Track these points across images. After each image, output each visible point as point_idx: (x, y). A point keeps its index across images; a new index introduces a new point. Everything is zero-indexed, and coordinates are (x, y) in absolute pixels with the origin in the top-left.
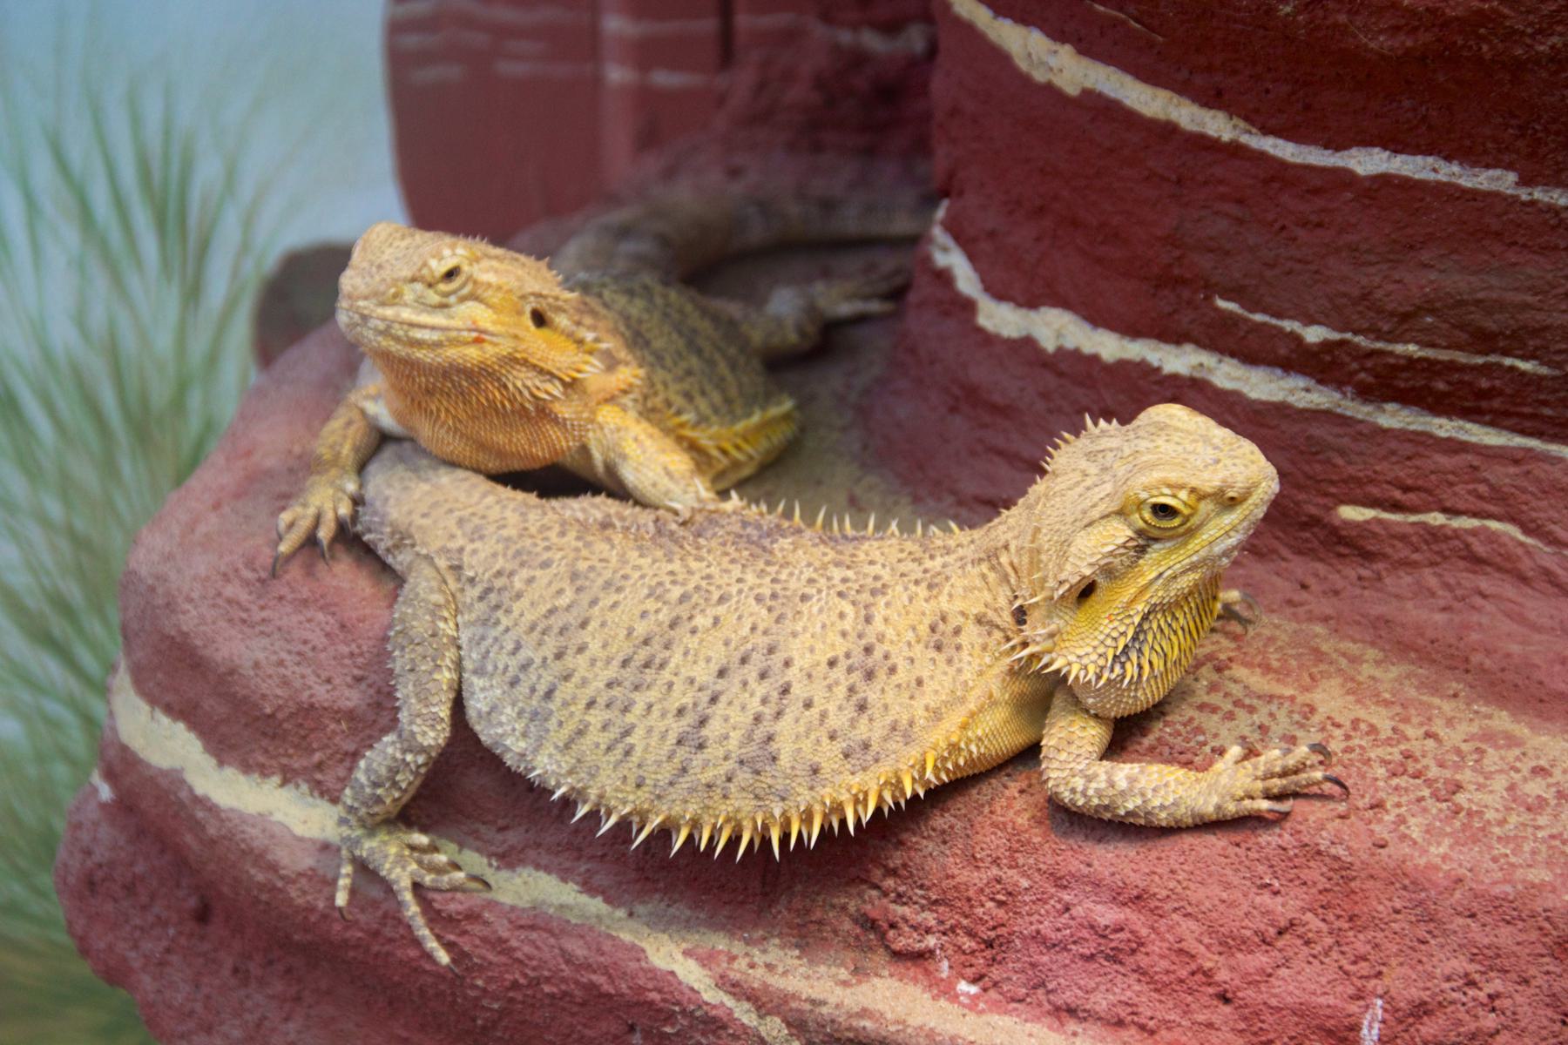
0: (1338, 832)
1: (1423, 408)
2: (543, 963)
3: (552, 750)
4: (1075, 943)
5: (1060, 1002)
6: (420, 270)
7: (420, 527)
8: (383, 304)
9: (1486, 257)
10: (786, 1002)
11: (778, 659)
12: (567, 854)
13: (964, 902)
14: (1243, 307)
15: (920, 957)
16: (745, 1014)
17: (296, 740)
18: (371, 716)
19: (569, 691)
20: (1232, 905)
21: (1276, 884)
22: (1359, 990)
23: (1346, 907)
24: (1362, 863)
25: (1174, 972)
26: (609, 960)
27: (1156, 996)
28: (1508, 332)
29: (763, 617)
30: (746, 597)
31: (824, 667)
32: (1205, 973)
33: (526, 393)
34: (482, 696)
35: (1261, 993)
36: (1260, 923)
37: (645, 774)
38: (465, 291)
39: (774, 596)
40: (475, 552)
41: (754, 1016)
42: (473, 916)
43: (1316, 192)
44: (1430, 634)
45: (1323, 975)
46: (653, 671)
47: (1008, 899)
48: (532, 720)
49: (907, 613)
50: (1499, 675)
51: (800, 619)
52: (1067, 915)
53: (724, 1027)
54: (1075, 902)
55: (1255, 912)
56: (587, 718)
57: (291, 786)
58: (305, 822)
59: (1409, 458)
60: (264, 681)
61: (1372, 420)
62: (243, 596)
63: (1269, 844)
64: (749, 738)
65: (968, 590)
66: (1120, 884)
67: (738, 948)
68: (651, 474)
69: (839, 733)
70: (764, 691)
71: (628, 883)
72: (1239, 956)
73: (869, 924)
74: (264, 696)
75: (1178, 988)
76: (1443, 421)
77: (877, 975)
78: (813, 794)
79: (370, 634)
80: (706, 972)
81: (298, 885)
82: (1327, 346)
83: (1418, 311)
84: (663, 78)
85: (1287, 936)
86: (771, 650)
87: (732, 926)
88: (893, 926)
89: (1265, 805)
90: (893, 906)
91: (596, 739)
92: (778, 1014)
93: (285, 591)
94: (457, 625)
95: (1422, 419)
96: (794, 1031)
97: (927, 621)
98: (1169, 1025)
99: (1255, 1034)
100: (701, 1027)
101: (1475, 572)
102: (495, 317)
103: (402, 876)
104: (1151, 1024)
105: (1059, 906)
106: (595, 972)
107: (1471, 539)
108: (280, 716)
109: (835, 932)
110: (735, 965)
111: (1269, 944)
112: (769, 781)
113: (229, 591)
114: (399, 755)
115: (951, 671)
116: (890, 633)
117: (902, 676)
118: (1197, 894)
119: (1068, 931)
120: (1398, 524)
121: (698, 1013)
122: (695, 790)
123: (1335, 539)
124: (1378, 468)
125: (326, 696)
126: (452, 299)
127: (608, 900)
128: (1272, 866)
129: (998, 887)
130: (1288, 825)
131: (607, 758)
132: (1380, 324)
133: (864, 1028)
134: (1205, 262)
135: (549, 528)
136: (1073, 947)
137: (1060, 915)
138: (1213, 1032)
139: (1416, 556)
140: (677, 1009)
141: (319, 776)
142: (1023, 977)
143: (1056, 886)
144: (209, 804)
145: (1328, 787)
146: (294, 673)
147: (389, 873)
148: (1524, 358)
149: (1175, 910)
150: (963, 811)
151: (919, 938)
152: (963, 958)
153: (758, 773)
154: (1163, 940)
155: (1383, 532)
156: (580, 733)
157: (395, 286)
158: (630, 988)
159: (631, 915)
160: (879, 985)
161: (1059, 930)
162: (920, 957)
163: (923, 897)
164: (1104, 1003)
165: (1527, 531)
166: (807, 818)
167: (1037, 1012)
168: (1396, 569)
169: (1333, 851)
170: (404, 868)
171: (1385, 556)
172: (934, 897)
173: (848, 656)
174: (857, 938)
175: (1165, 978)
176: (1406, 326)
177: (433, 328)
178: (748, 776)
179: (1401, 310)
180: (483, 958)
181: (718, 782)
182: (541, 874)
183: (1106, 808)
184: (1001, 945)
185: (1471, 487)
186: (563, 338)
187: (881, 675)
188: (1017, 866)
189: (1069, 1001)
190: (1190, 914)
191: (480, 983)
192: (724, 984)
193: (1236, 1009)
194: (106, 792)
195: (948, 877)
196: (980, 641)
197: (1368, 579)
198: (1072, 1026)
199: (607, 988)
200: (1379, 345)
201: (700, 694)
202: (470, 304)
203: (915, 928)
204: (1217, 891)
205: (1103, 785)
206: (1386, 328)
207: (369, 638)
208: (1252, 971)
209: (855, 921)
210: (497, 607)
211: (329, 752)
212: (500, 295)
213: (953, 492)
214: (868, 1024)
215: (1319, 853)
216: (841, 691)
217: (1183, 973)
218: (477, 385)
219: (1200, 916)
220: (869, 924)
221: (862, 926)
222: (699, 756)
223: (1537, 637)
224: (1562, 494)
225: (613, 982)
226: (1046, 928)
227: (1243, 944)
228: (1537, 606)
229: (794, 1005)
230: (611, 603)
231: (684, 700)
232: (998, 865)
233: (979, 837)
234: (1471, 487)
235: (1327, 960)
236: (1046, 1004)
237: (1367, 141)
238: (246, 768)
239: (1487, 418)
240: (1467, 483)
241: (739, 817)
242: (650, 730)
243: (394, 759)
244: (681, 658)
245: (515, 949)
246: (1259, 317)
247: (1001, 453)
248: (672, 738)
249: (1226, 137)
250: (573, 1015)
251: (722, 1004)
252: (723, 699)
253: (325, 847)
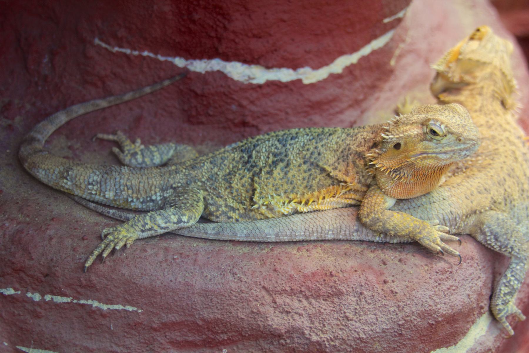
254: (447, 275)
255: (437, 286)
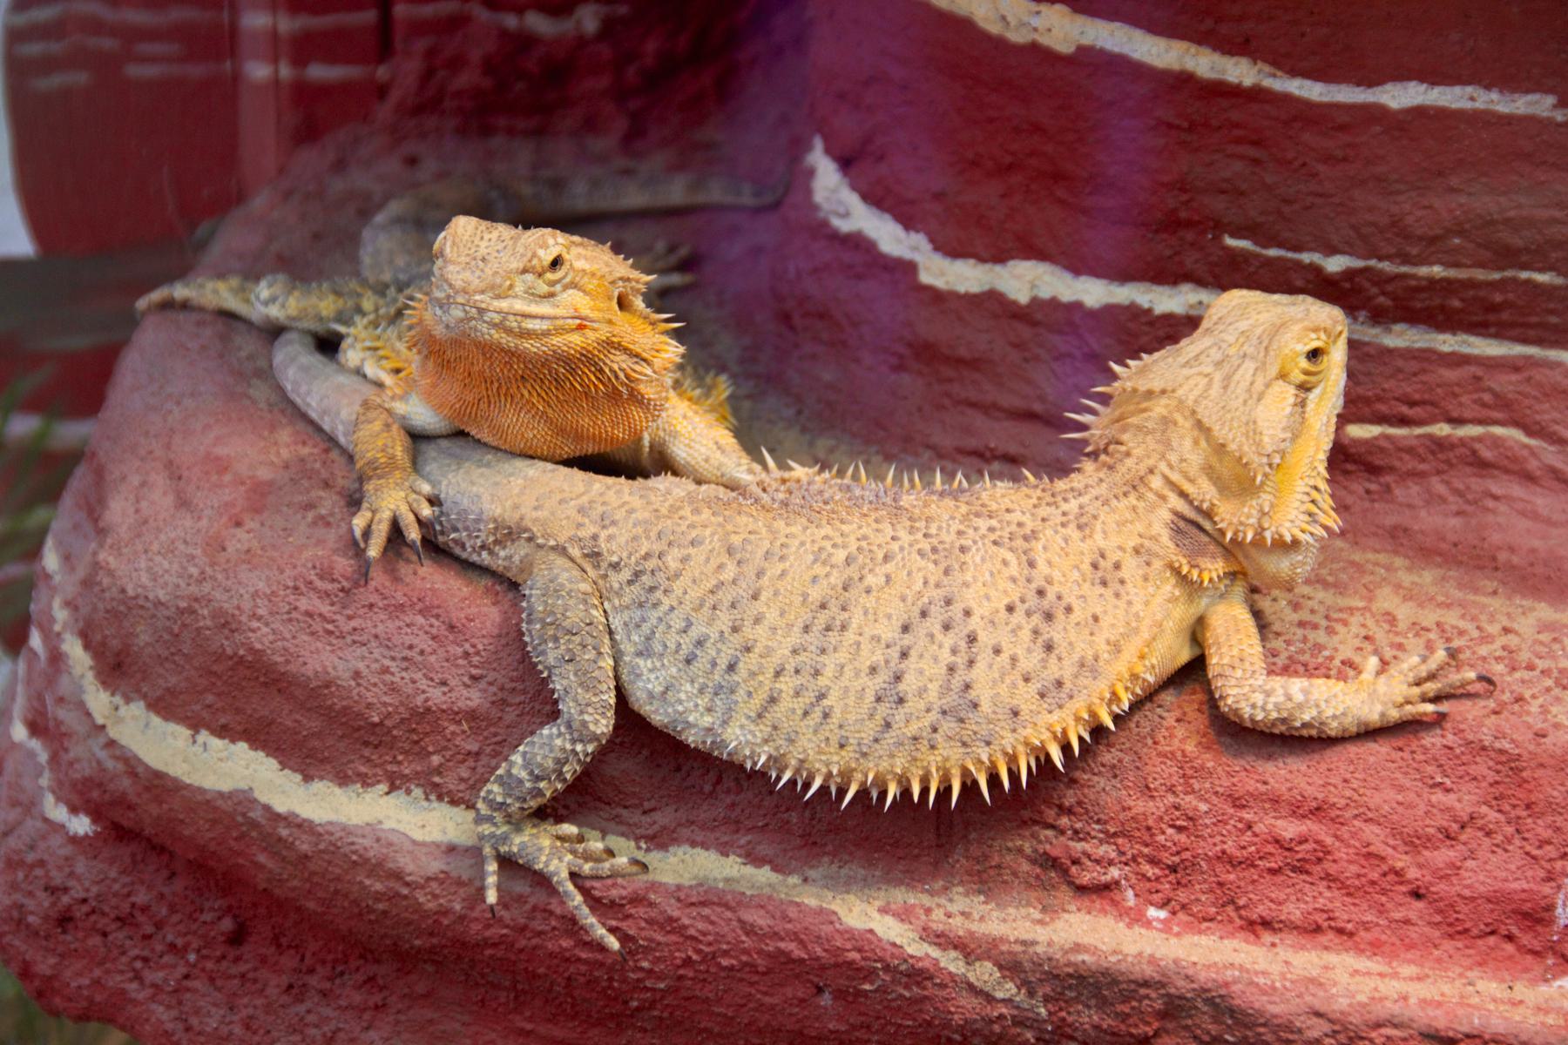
0: (1498, 729)
1: (1430, 326)
2: (720, 937)
3: (744, 721)
4: (1260, 858)
5: (1255, 917)
6: (530, 261)
7: (536, 520)
8: (498, 297)
9: (1515, 178)
10: (996, 946)
11: (957, 609)
12: (723, 828)
13: (1143, 831)
14: (1256, 243)
15: (1105, 889)
16: (951, 962)
17: (407, 746)
18: (495, 713)
19: (754, 661)
20: (1411, 806)
21: (1448, 782)
22: (1549, 872)
23: (1521, 796)
24: (1530, 753)
25: (1365, 875)
26: (798, 926)
27: (1348, 900)
28: (1533, 247)
29: (934, 573)
30: (909, 554)
31: (1003, 613)
32: (1397, 873)
33: (622, 375)
34: (652, 676)
35: (1453, 885)
36: (1442, 820)
37: (848, 734)
38: (567, 280)
39: (934, 550)
40: (610, 538)
41: (961, 963)
42: (637, 900)
43: (1342, 128)
44: (1451, 537)
45: (1511, 863)
46: (836, 633)
47: (1188, 823)
48: (716, 694)
49: (1067, 555)
50: (1529, 569)
51: (968, 569)
52: (1249, 833)
53: (931, 978)
54: (1256, 819)
55: (1435, 811)
56: (777, 685)
57: (401, 792)
58: (424, 826)
59: (1415, 374)
60: (369, 690)
61: (1378, 341)
62: (325, 609)
63: (1433, 744)
64: (946, 689)
65: (1121, 524)
66: (1299, 798)
67: (926, 900)
68: (703, 450)
69: (1033, 675)
70: (952, 642)
71: (792, 849)
72: (1426, 853)
73: (1049, 862)
74: (369, 706)
75: (1371, 890)
76: (1447, 337)
77: (1064, 911)
78: (1016, 736)
79: (484, 632)
80: (906, 926)
81: (428, 890)
82: (1349, 274)
83: (1449, 232)
84: (319, 72)
85: (1469, 830)
86: (948, 602)
87: (911, 879)
88: (1075, 862)
89: (1430, 708)
90: (1072, 844)
91: (790, 705)
92: (989, 958)
93: (374, 598)
94: (605, 611)
95: (1427, 337)
96: (1007, 973)
97: (1087, 560)
98: (1366, 926)
99: (1450, 925)
100: (904, 980)
101: (1482, 476)
102: (592, 303)
103: (558, 866)
104: (1350, 926)
105: (1240, 825)
106: (782, 939)
107: (1477, 446)
108: (388, 723)
109: (1015, 874)
110: (934, 917)
111: (1453, 839)
112: (974, 727)
113: (303, 604)
114: (568, 746)
115: (1122, 604)
116: (1057, 575)
117: (1077, 615)
118: (1375, 799)
119: (1253, 848)
120: (1405, 437)
121: (903, 967)
122: (902, 744)
123: (1342, 457)
124: (1386, 386)
125: (444, 699)
126: (558, 287)
127: (776, 869)
128: (1440, 766)
129: (1177, 813)
130: (1448, 725)
131: (806, 722)
132: (1408, 248)
133: (1084, 962)
134: (1217, 205)
135: (680, 508)
136: (1260, 863)
137: (1243, 834)
138: (1411, 928)
139: (1422, 467)
140: (879, 965)
141: (437, 779)
142: (1212, 897)
143: (1234, 806)
144: (298, 821)
145: (1479, 687)
146: (403, 678)
147: (547, 864)
148: (1541, 270)
149: (1356, 816)
150: (1128, 745)
151: (1103, 871)
152: (1148, 885)
153: (962, 721)
154: (1349, 846)
155: (1390, 447)
156: (773, 700)
157: (510, 278)
158: (826, 950)
159: (805, 880)
160: (1072, 920)
161: (1244, 848)
162: (1105, 889)
163: (1101, 831)
164: (1298, 912)
165: (1529, 432)
166: (1012, 759)
167: (1230, 928)
168: (1404, 480)
169: (1497, 745)
170: (560, 859)
171: (1392, 469)
172: (1112, 830)
173: (1023, 601)
174: (1037, 877)
175: (1357, 883)
176: (1433, 249)
177: (542, 318)
178: (953, 725)
179: (1431, 233)
180: (651, 940)
181: (924, 734)
182: (698, 850)
183: (1284, 721)
184: (1186, 868)
185: (1476, 396)
186: (641, 320)
187: (1060, 615)
188: (1193, 792)
189: (1264, 914)
190: (1371, 819)
191: (645, 964)
192: (928, 936)
193: (1430, 903)
194: (81, 825)
195: (1124, 809)
196: (1141, 572)
197: (1375, 492)
198: (1268, 937)
199: (798, 953)
200: (1404, 269)
201: (889, 651)
202: (571, 291)
203: (1097, 862)
204: (1391, 794)
205: (1281, 699)
206: (1414, 251)
207: (484, 636)
208: (1441, 865)
209: (1033, 862)
210: (652, 589)
211: (448, 754)
212: (595, 282)
213: (928, 447)
214: (1086, 957)
215: (1484, 748)
216: (1026, 634)
217: (1375, 875)
218: (573, 371)
219: (1382, 820)
220: (1050, 862)
221: (1041, 866)
222: (901, 711)
223: (1554, 532)
224: (1563, 396)
225: (805, 947)
226: (1230, 846)
227: (1427, 842)
228: (1543, 501)
229: (1004, 948)
230: (779, 572)
231: (874, 658)
232: (1174, 793)
233: (1149, 768)
234: (1476, 396)
235: (1510, 848)
236: (1237, 920)
237: (1401, 74)
238: (343, 780)
239: (1492, 330)
240: (1470, 393)
241: (948, 765)
242: (846, 690)
243: (563, 750)
244: (862, 618)
245: (685, 927)
246: (1273, 252)
247: (973, 405)
248: (870, 697)
249: (1248, 82)
250: (752, 984)
251: (927, 955)
252: (913, 653)
253: (451, 849)
254: (329, 586)
255: (288, 588)
